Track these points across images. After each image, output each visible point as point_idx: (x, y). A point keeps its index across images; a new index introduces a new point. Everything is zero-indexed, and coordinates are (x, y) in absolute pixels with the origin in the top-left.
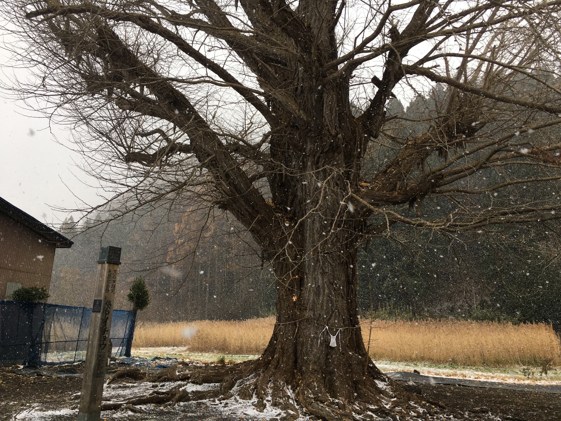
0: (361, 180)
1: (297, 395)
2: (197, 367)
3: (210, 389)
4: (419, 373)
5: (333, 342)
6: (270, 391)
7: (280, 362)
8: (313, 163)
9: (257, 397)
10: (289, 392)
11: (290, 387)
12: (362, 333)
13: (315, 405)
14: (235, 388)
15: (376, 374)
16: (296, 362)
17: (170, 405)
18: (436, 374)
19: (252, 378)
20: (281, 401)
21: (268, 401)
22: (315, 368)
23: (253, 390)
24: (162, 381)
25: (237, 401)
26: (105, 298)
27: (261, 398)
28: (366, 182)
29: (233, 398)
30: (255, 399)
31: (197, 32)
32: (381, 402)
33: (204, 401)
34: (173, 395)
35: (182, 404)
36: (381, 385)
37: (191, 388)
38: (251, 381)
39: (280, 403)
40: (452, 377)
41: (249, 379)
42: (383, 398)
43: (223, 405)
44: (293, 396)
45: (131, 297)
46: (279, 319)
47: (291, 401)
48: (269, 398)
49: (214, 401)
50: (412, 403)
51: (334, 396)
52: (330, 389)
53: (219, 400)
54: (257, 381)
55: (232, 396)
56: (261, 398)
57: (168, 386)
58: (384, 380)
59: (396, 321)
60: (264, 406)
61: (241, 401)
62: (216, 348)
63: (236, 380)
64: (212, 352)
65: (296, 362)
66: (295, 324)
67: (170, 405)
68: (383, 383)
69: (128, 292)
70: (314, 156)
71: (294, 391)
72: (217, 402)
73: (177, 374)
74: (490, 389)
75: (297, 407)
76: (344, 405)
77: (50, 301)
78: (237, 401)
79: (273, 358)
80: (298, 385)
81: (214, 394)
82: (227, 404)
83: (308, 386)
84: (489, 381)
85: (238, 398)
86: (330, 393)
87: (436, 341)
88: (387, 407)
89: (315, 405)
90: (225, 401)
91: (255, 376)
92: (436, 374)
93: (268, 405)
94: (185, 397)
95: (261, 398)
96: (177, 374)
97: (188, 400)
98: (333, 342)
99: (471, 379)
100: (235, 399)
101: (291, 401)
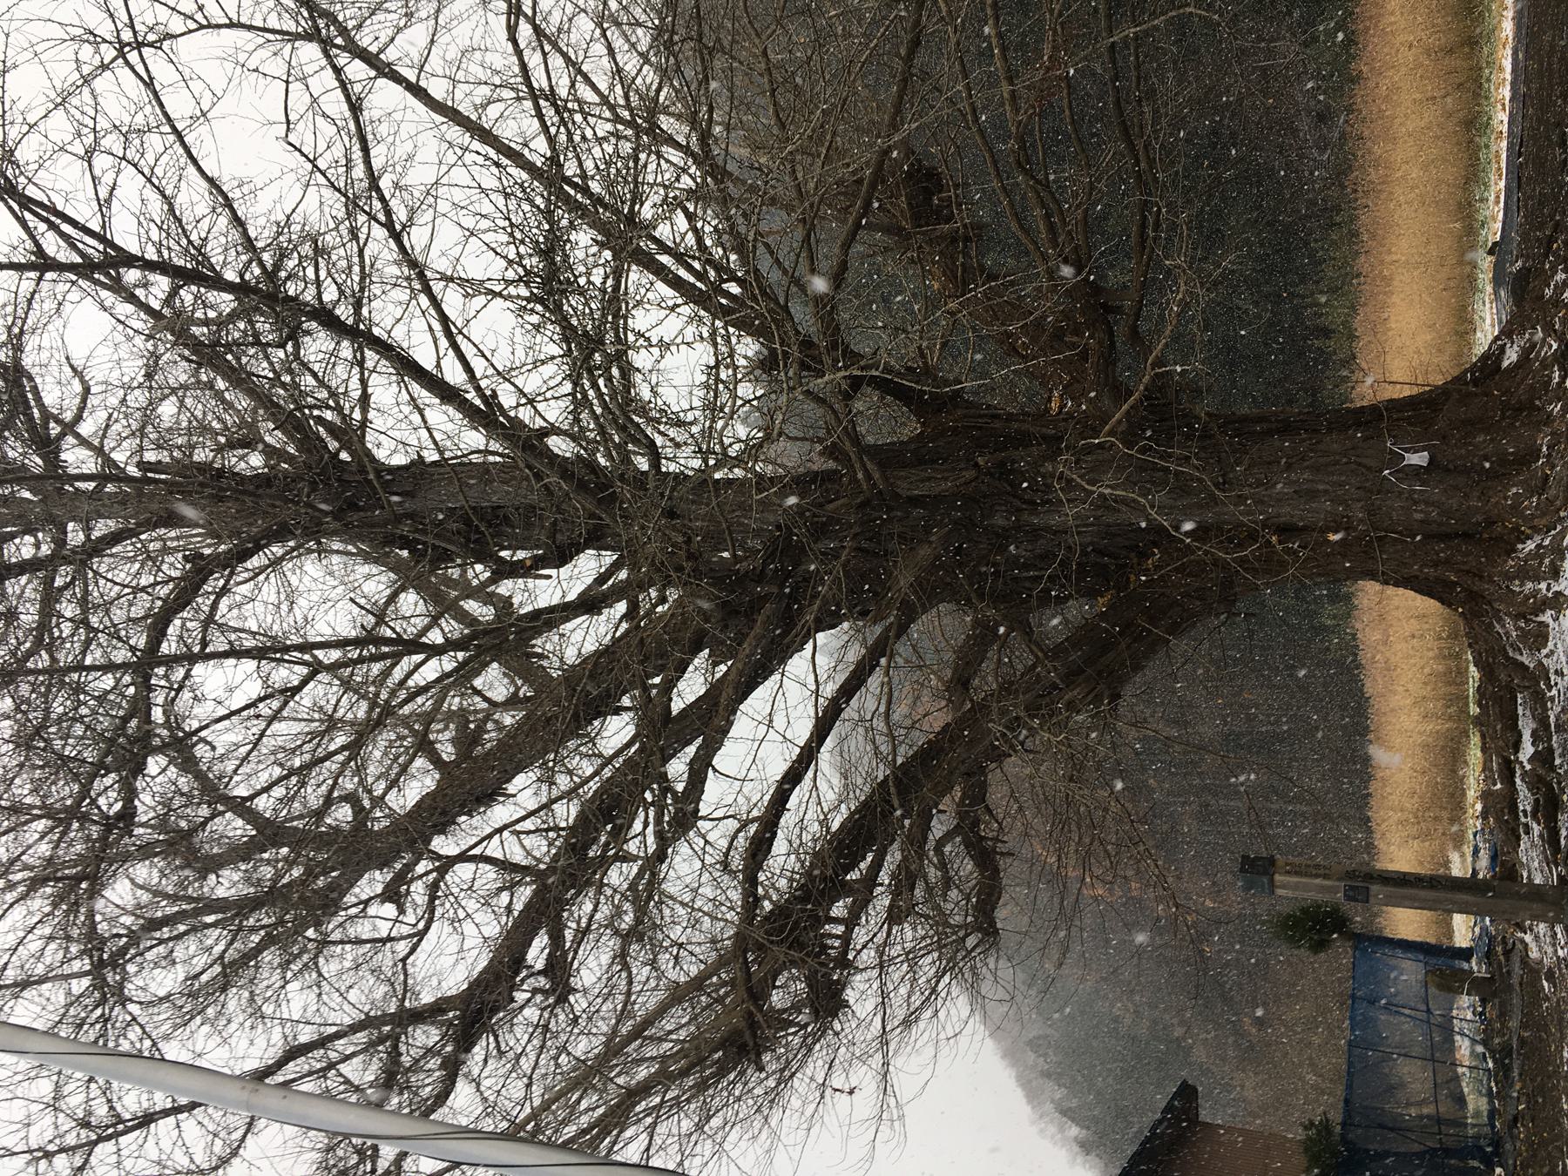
0: (1047, 410)
1: (1536, 530)
2: (1484, 744)
3: (1528, 713)
4: (1495, 244)
5: (1419, 459)
6: (1529, 585)
7: (1466, 568)
8: (1034, 512)
9: (1543, 612)
10: (1530, 546)
11: (1520, 546)
12: (1395, 396)
13: (1553, 492)
14: (1525, 659)
15: (1492, 358)
16: (1466, 536)
17: (1559, 783)
18: (1497, 202)
19: (1503, 626)
20: (1547, 561)
21: (1548, 589)
22: (1476, 494)
23: (1527, 621)
24: (1517, 818)
25: (1552, 652)
26: (1339, 879)
27: (1544, 604)
28: (1049, 400)
29: (1545, 661)
30: (1547, 617)
31: (715, 770)
32: (1545, 358)
33: (1552, 719)
34: (1540, 779)
35: (1558, 762)
36: (1511, 356)
37: (1527, 750)
38: (1509, 628)
39: (1552, 562)
40: (1504, 165)
41: (1507, 634)
42: (1539, 352)
43: (1559, 680)
44: (1538, 539)
45: (1320, 946)
46: (1372, 575)
47: (1547, 542)
48: (1543, 586)
49: (1552, 699)
50: (1548, 292)
51: (1537, 454)
52: (1522, 464)
53: (1550, 688)
54: (1508, 614)
55: (1540, 663)
56: (1544, 603)
57: (1525, 801)
58: (1502, 349)
59: (1358, 276)
60: (1559, 594)
61: (1550, 645)
62: (1454, 771)
63: (1508, 658)
64: (1462, 781)
65: (1466, 536)
66: (1380, 539)
67: (1559, 783)
68: (1508, 351)
69: (1304, 953)
70: (1019, 510)
71: (1529, 537)
72: (1554, 692)
73: (1499, 786)
74: (1527, 82)
75: (1559, 528)
76: (1552, 434)
77: (1336, 1116)
78: (1552, 652)
79: (1456, 583)
80: (1516, 528)
81: (1539, 701)
82: (1556, 672)
83: (1515, 508)
84: (1509, 77)
85: (1544, 652)
86: (1530, 463)
87: (1415, 173)
88: (1555, 346)
89: (1553, 492)
90: (1553, 677)
91: (1500, 620)
92: (1497, 202)
93: (1556, 588)
94: (1544, 758)
95: (1544, 604)
96: (1499, 786)
97: (1551, 750)
98: (1419, 459)
99: (1506, 120)
100: (1547, 656)
101: (1547, 542)
